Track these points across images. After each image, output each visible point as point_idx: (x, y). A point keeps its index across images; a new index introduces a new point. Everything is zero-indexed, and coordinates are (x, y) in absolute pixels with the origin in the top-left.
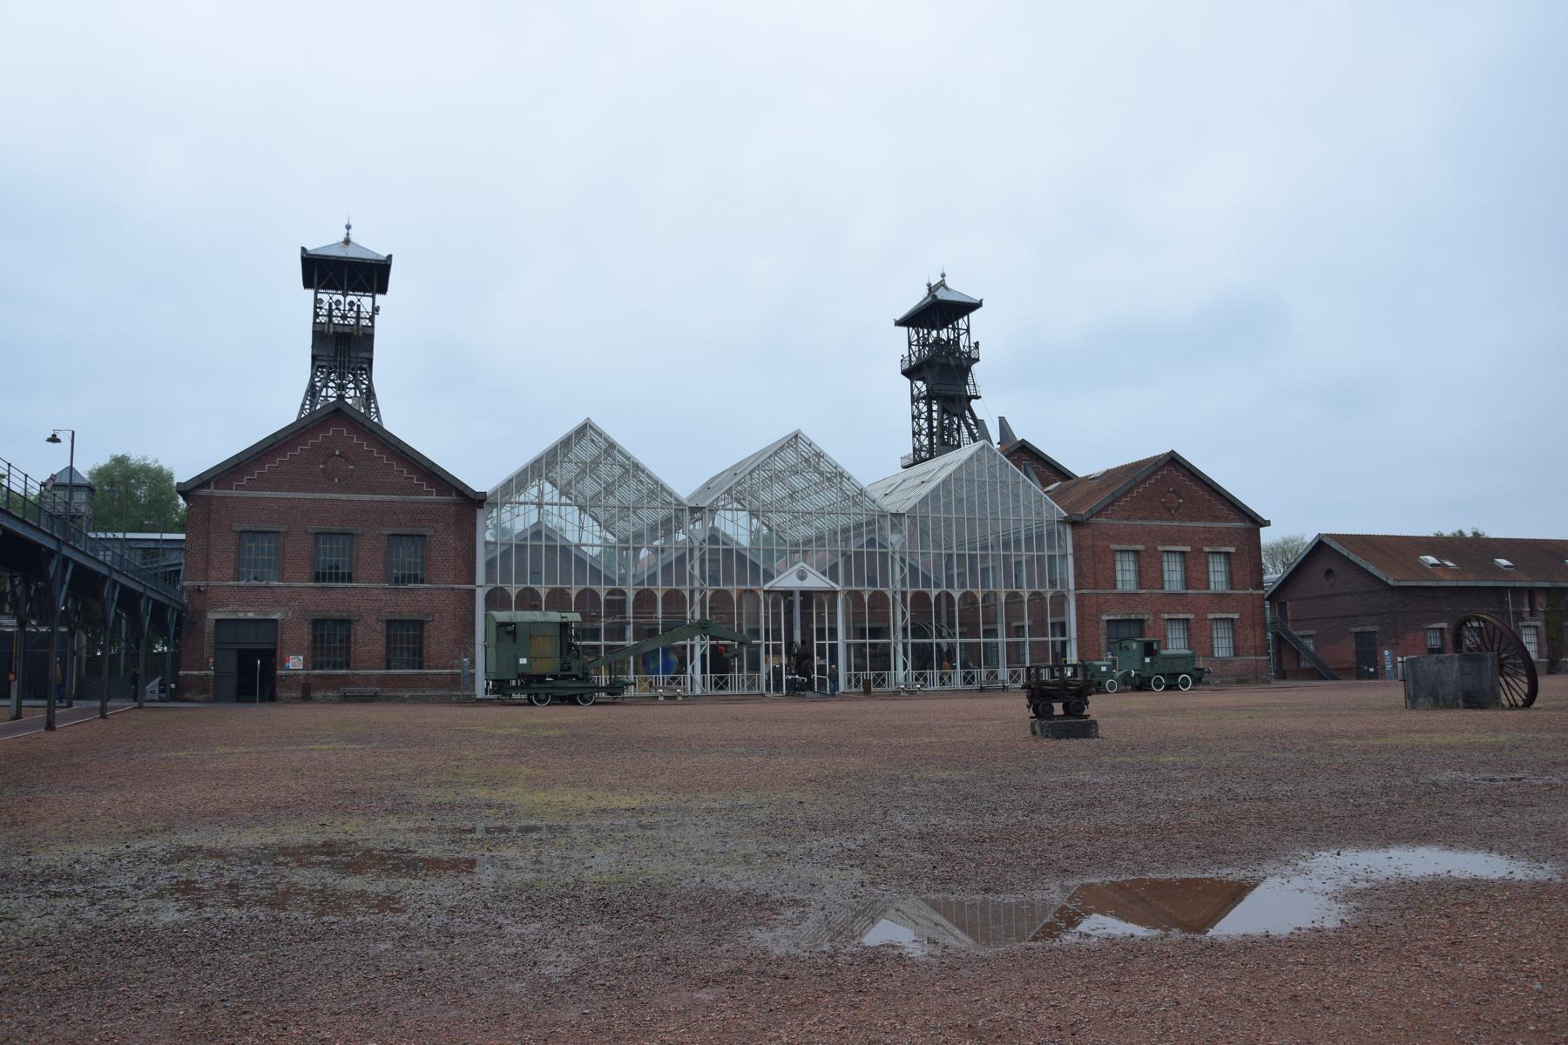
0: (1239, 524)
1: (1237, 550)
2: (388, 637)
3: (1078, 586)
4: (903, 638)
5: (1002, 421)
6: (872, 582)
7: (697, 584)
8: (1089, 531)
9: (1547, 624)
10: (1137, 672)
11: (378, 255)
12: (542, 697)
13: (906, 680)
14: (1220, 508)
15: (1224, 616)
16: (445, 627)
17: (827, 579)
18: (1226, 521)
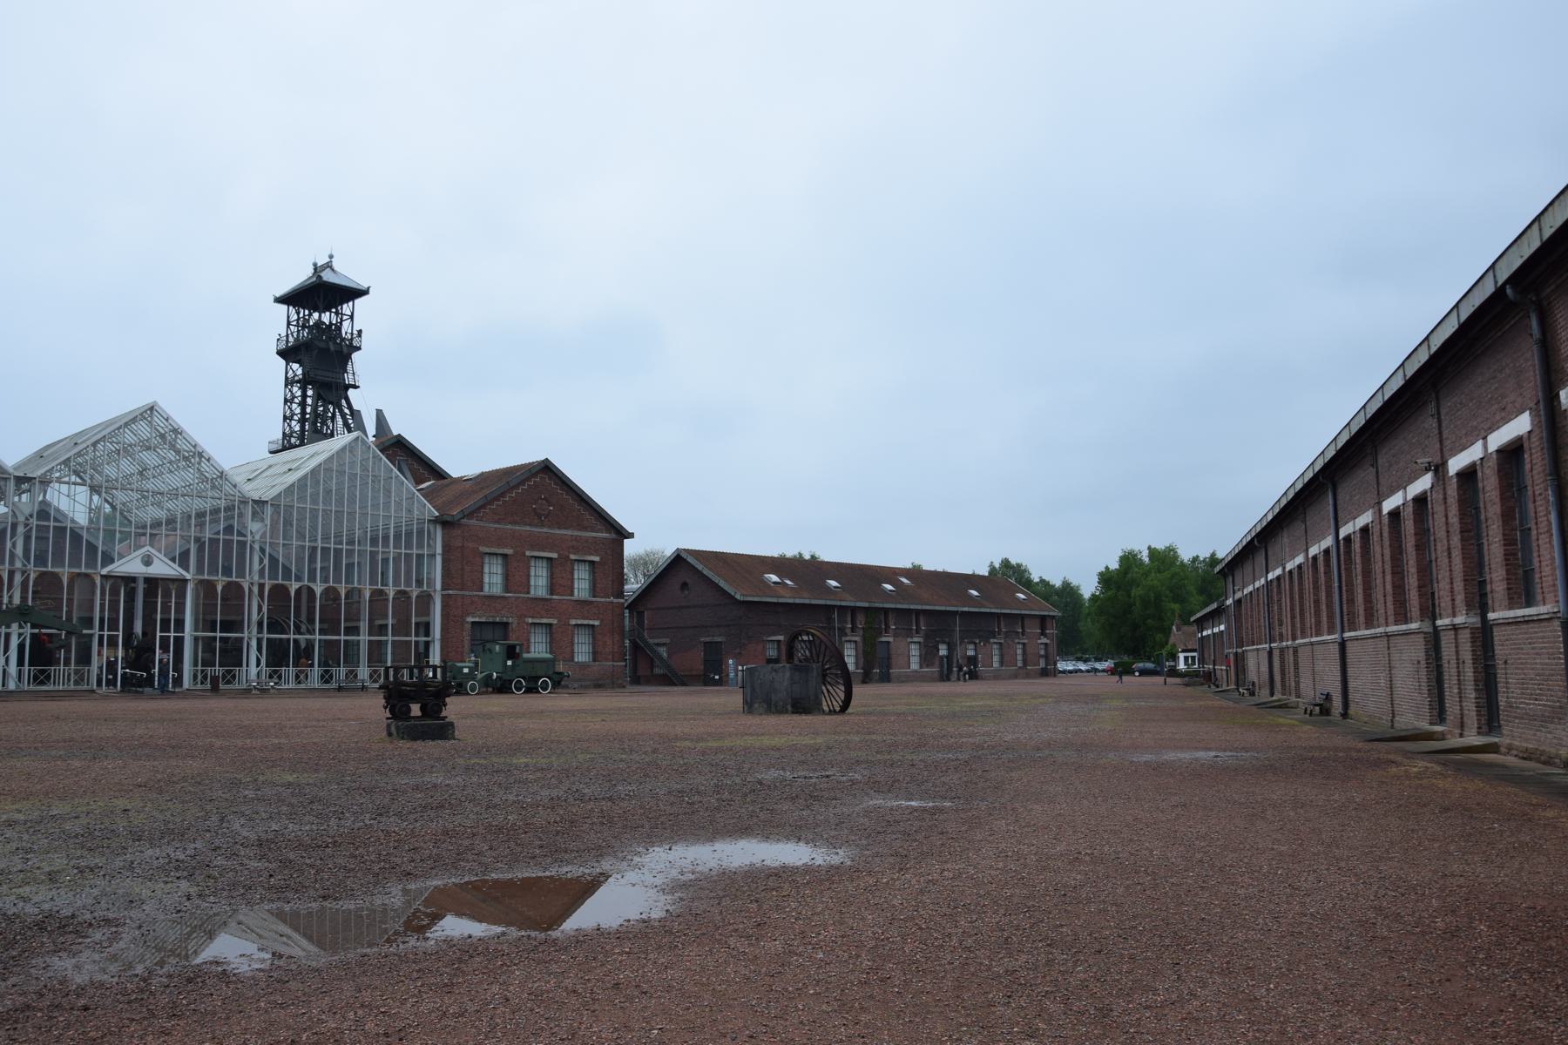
1: (601, 559)
4: (258, 633)
5: (379, 414)
6: (227, 571)
7: (18, 564)
8: (459, 532)
9: (864, 638)
14: (589, 518)
15: (586, 622)
17: (176, 566)
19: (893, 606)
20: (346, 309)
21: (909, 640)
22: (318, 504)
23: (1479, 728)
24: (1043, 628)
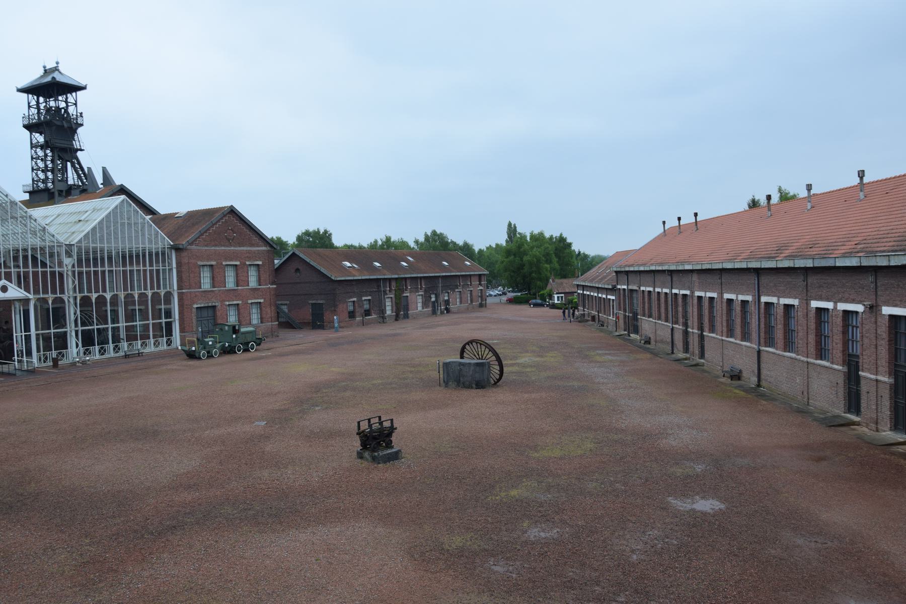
1: (263, 263)
3: (180, 287)
4: (75, 327)
6: (54, 291)
8: (186, 254)
9: (396, 295)
10: (229, 344)
14: (255, 239)
15: (256, 301)
17: (22, 291)
19: (409, 276)
20: (71, 99)
21: (417, 294)
23: (891, 428)
24: (480, 281)
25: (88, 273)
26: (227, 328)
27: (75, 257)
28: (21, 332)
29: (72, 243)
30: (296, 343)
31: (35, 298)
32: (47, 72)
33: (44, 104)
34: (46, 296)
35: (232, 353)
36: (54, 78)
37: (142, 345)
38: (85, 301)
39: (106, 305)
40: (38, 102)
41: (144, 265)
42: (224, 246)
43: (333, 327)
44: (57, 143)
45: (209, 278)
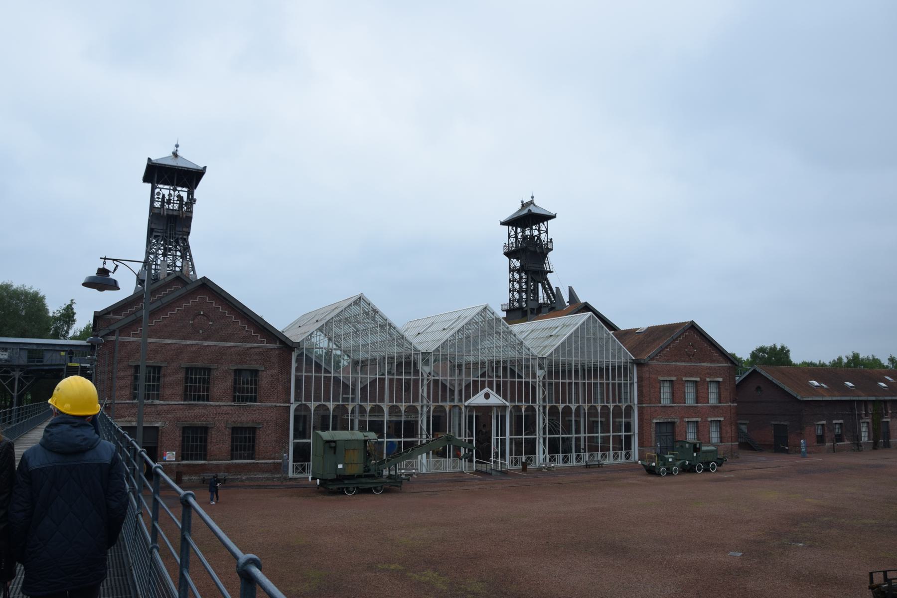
0: (725, 365)
2: (233, 438)
3: (640, 402)
5: (571, 289)
6: (527, 401)
7: (425, 402)
8: (647, 369)
11: (197, 166)
12: (351, 489)
13: (544, 461)
14: (716, 355)
15: (716, 419)
16: (270, 432)
17: (501, 398)
18: (718, 363)
22: (578, 357)
25: (557, 384)
26: (687, 445)
27: (546, 369)
28: (465, 437)
29: (544, 356)
30: (759, 467)
31: (511, 406)
32: (524, 206)
33: (521, 234)
34: (520, 404)
35: (692, 472)
36: (530, 210)
37: (602, 457)
38: (553, 411)
39: (571, 416)
40: (516, 233)
41: (608, 379)
42: (684, 362)
43: (800, 452)
44: (531, 267)
45: (669, 393)
